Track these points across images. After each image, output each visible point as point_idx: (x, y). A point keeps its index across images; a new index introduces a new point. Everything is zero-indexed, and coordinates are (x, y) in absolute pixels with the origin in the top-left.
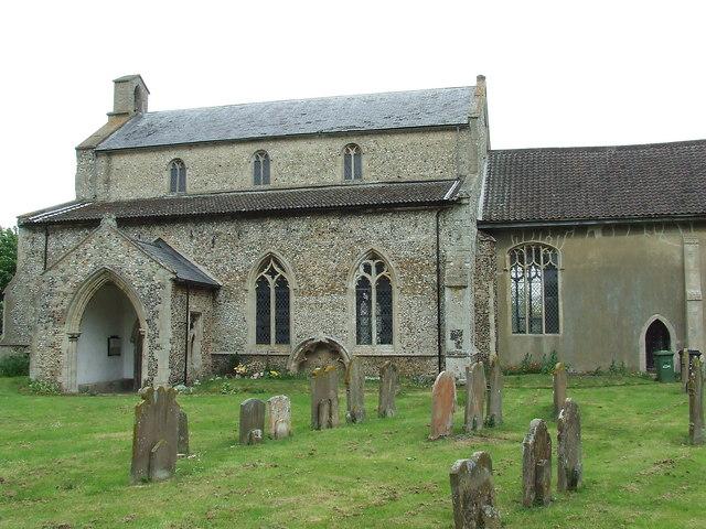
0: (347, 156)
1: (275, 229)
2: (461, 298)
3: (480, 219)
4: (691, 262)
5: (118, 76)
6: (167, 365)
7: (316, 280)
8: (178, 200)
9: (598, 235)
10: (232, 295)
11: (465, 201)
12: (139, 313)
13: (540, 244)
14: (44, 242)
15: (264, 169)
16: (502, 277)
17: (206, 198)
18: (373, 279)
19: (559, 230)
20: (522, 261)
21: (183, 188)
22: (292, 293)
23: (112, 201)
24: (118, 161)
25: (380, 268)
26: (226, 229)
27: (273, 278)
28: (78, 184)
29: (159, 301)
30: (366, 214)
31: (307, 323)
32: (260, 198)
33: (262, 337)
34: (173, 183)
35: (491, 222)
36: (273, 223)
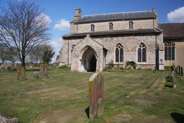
1: (120, 38)
6: (102, 66)
7: (129, 49)
18: (142, 49)
21: (94, 30)
26: (109, 39)
31: (127, 57)
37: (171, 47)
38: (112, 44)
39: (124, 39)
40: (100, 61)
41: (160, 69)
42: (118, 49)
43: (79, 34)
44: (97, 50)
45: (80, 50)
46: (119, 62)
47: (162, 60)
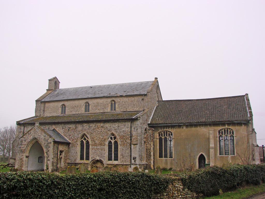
0: (112, 104)
1: (86, 126)
4: (211, 137)
7: (97, 142)
10: (73, 146)
11: (139, 119)
13: (167, 131)
14: (23, 129)
18: (113, 141)
21: (65, 113)
24: (47, 105)
26: (72, 126)
30: (119, 122)
32: (87, 117)
33: (82, 158)
34: (62, 111)
36: (85, 125)
37: (163, 138)
38: (76, 135)
39: (91, 128)
40: (49, 158)
42: (111, 142)
44: (46, 144)
46: (84, 160)
47: (136, 158)
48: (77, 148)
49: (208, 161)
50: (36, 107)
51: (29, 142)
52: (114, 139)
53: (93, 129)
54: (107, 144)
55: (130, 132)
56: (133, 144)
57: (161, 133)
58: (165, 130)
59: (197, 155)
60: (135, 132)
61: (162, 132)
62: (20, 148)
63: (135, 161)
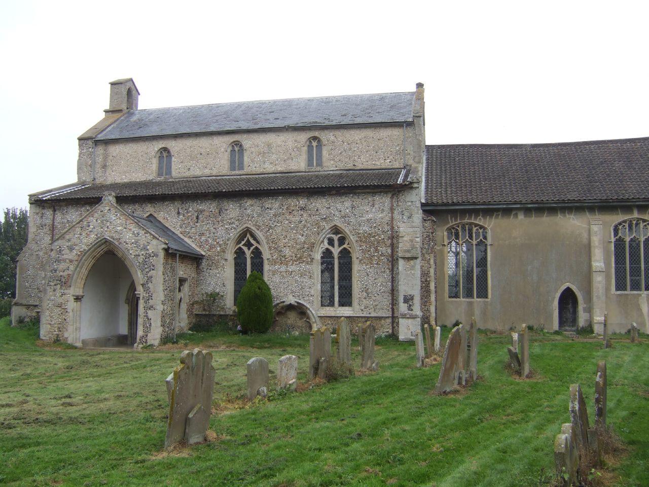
0: (310, 147)
1: (252, 207)
2: (413, 268)
3: (423, 201)
4: (596, 240)
5: (113, 80)
6: (159, 323)
7: (287, 252)
8: (165, 183)
9: (521, 216)
10: (214, 264)
11: (415, 185)
12: (135, 277)
13: (471, 224)
14: (51, 217)
15: (239, 157)
16: (442, 252)
17: (190, 181)
18: (336, 251)
19: (489, 211)
20: (457, 237)
21: (169, 172)
22: (266, 262)
23: (108, 183)
24: (114, 150)
25: (342, 241)
26: (209, 207)
27: (249, 249)
28: (80, 169)
29: (153, 267)
35: (432, 204)
36: (249, 202)
38: (221, 232)
41: (402, 337)
42: (244, 253)
43: (111, 185)
44: (141, 259)
45: (76, 258)
47: (412, 298)
48: (224, 271)
49: (585, 306)
50: (79, 156)
51: (85, 253)
52: (340, 245)
53: (275, 215)
54: (319, 258)
55: (389, 223)
56: (403, 258)
57: (454, 228)
58: (466, 221)
59: (556, 291)
60: (403, 225)
61: (458, 227)
62: (56, 271)
63: (410, 305)
